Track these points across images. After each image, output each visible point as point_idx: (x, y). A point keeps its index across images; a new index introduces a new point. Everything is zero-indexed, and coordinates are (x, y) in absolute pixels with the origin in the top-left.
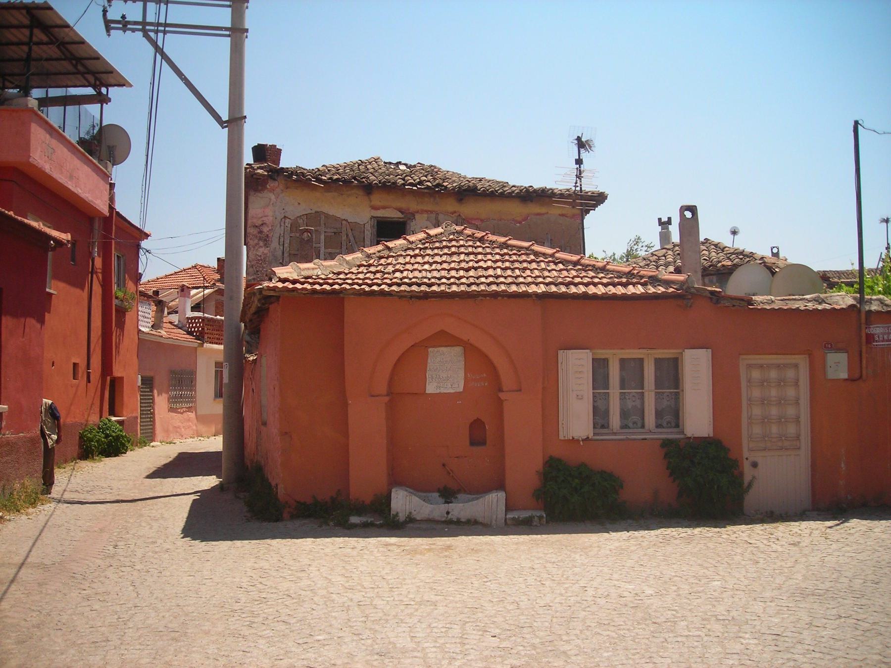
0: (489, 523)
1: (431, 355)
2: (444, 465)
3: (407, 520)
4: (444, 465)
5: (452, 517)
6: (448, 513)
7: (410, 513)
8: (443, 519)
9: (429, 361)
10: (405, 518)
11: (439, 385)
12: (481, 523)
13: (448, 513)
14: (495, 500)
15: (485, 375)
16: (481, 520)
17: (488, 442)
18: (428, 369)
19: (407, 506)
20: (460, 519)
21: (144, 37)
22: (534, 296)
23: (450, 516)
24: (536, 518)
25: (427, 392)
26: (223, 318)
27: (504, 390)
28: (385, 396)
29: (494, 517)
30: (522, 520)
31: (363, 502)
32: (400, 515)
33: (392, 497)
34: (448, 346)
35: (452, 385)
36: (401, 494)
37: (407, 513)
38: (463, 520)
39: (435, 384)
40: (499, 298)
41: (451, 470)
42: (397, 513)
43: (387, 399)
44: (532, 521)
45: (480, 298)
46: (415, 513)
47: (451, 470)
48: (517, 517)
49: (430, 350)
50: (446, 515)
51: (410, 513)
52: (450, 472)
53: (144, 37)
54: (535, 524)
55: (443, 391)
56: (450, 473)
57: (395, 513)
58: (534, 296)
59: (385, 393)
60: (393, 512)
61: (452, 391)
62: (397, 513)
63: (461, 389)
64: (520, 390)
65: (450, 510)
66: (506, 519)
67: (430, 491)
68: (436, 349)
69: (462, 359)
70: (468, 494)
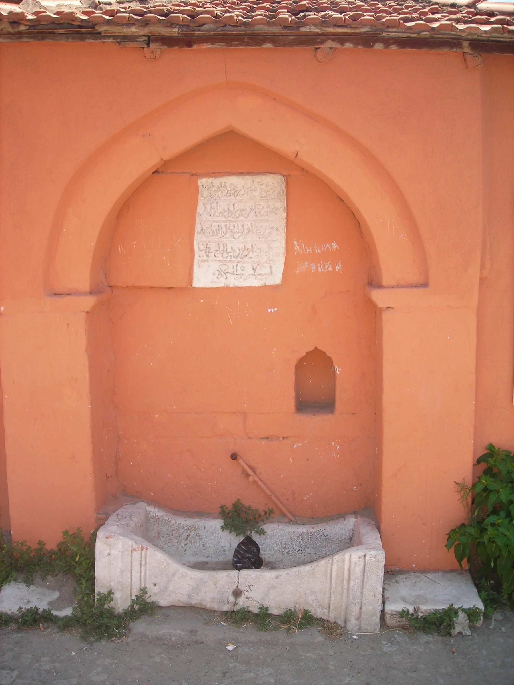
0: (340, 623)
1: (204, 195)
2: (234, 457)
3: (136, 607)
4: (234, 457)
5: (248, 603)
6: (237, 593)
7: (144, 591)
8: (226, 608)
9: (200, 208)
10: (129, 603)
11: (224, 268)
12: (321, 619)
13: (237, 593)
14: (358, 570)
15: (334, 245)
16: (318, 612)
17: (338, 405)
18: (198, 228)
19: (136, 576)
20: (267, 609)
21: (307, 353)
22: (465, 44)
23: (242, 602)
24: (462, 617)
25: (197, 283)
26: (269, 310)
27: (385, 283)
28: (85, 294)
29: (355, 610)
30: (424, 619)
31: (41, 543)
32: (117, 595)
33: (97, 552)
34: (249, 173)
35: (254, 270)
36: (121, 544)
37: (136, 592)
38: (275, 611)
39: (215, 266)
40: (379, 46)
41: (250, 467)
42: (110, 592)
43: (90, 302)
44: (451, 625)
45: (329, 44)
46: (156, 589)
47: (252, 468)
48: (411, 610)
49: (203, 182)
50: (232, 599)
51: (144, 591)
52: (250, 472)
53: (307, 353)
54: (458, 629)
55: (233, 282)
56: (248, 475)
57: (105, 591)
58: (465, 44)
59: (86, 286)
60: (100, 588)
61: (256, 283)
62: (110, 592)
63: (277, 279)
64: (425, 285)
65: (242, 588)
66: (383, 611)
67: (200, 514)
68: (217, 181)
69: (281, 205)
70: (290, 522)
